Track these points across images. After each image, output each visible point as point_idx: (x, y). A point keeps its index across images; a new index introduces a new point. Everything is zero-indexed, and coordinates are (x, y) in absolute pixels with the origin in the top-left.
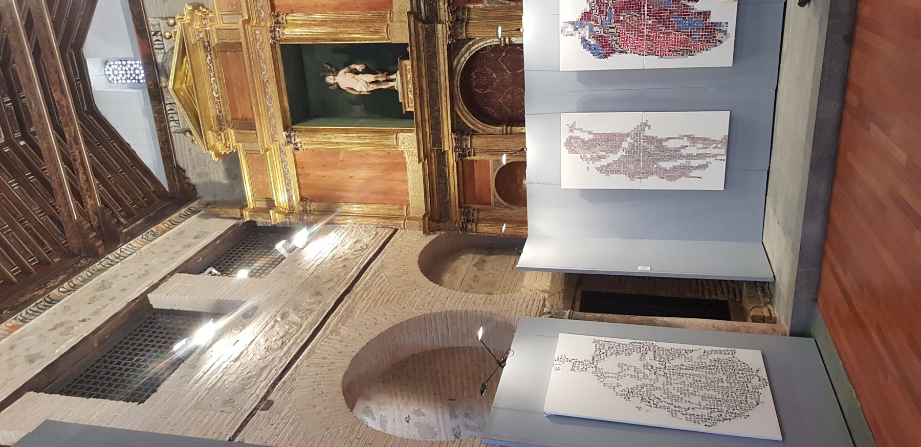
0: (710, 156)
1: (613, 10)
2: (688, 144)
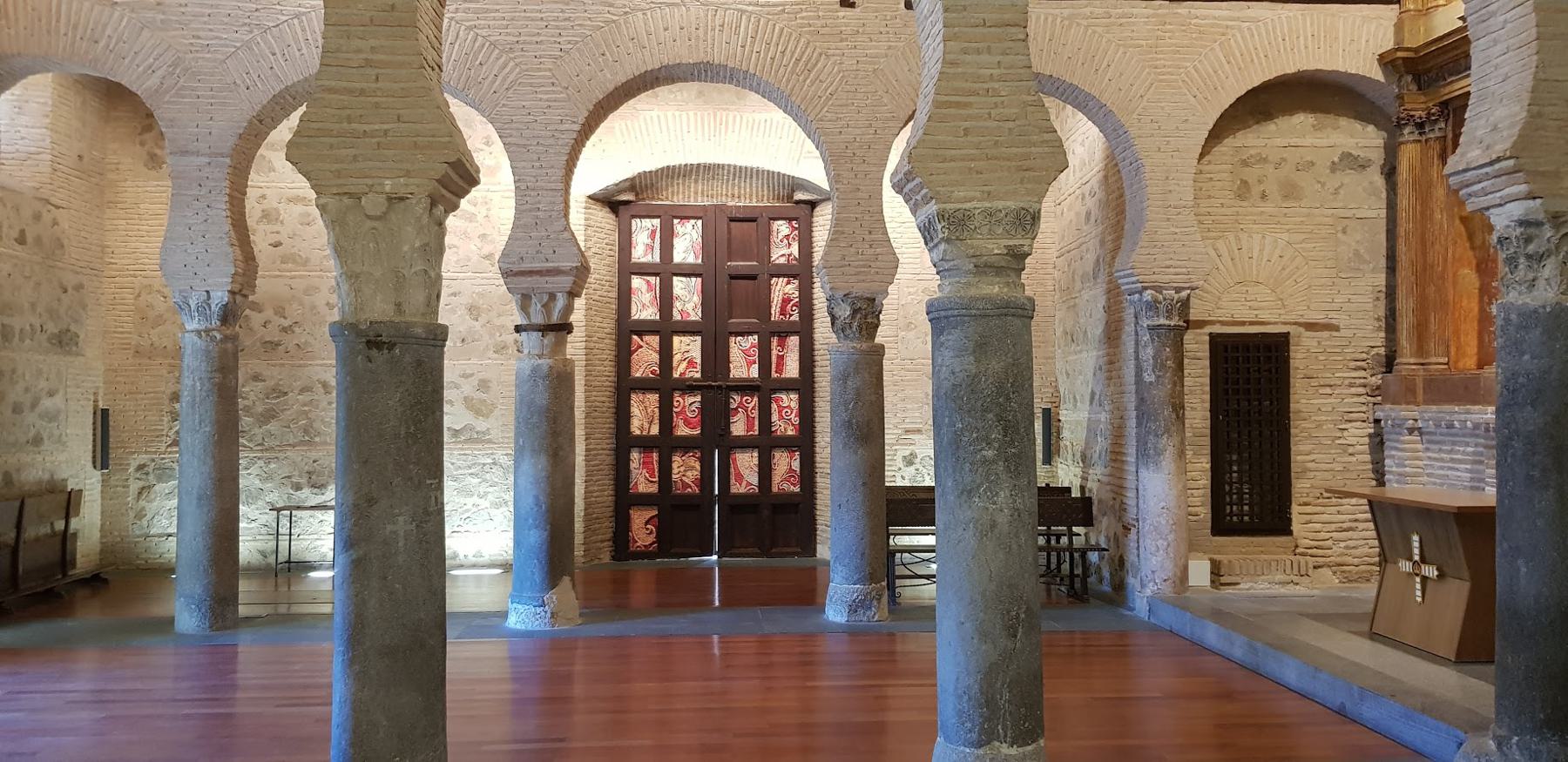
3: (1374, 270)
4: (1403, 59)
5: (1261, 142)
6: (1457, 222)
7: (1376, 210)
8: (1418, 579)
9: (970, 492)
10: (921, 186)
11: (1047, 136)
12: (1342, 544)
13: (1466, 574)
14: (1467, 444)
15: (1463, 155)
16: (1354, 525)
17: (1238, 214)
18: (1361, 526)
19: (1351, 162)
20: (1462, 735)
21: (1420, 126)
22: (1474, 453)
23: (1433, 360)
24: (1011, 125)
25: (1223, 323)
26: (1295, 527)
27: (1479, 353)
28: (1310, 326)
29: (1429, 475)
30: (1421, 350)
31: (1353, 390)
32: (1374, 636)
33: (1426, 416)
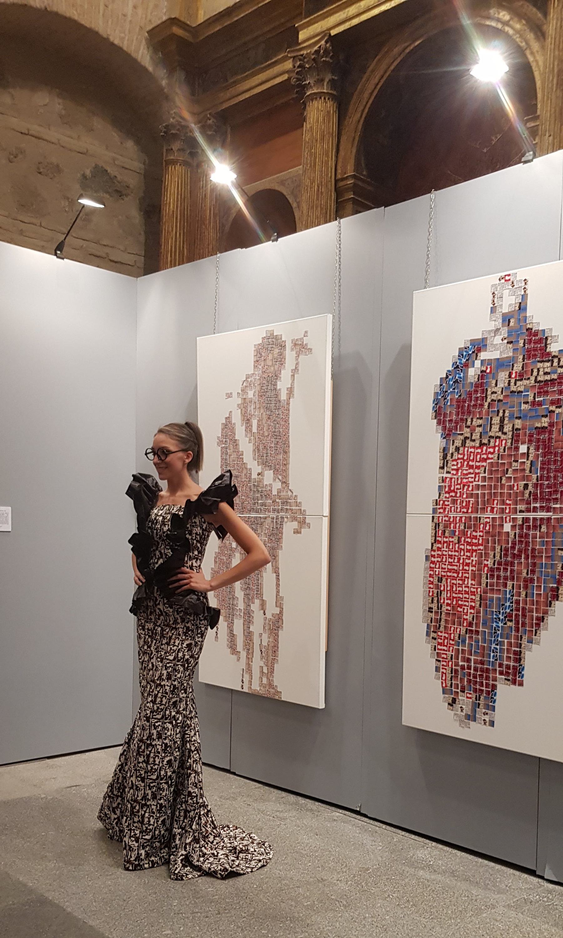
0: (249, 658)
1: (545, 422)
2: (269, 616)
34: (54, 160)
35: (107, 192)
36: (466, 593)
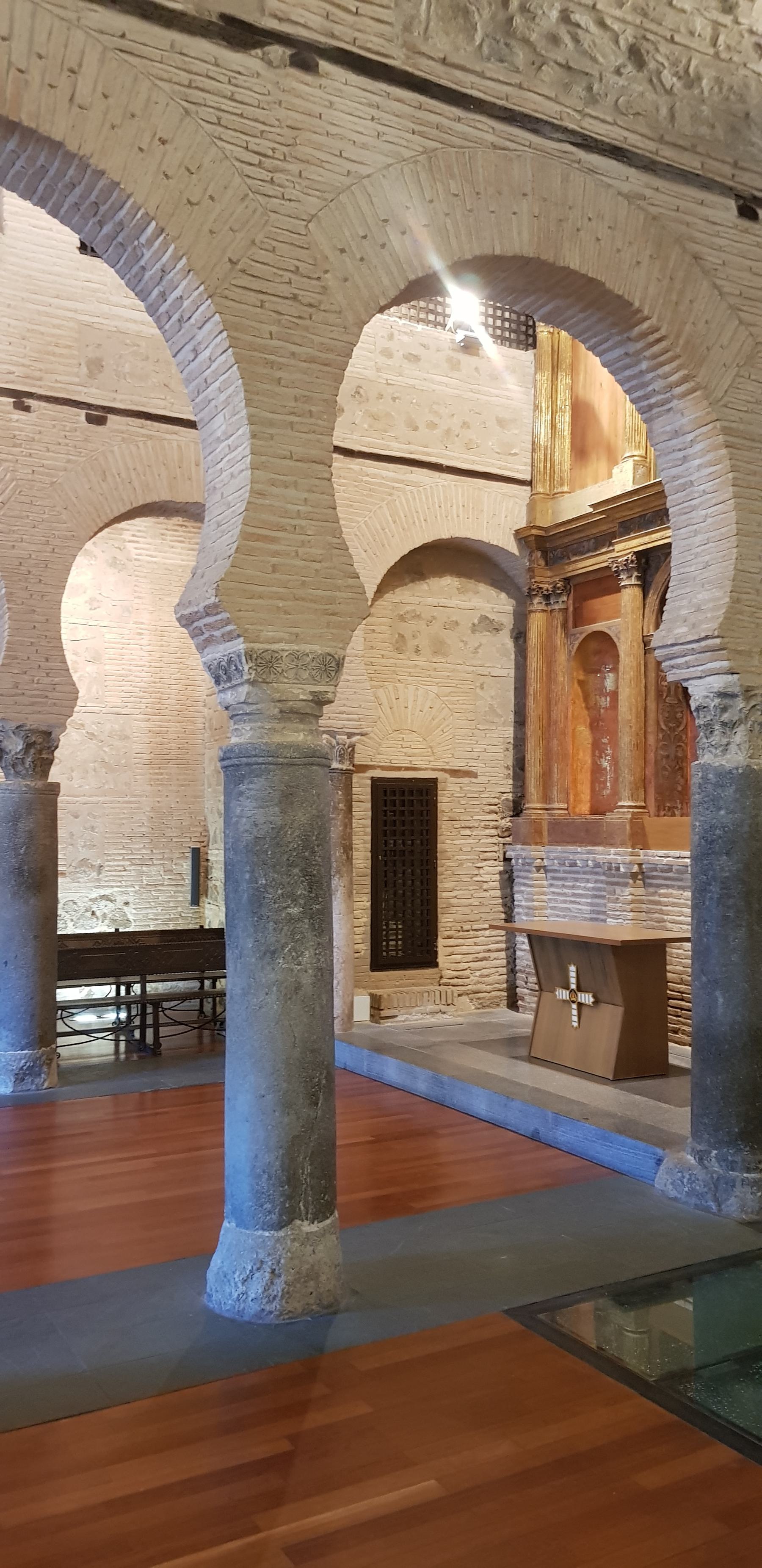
3: (504, 724)
4: (536, 536)
5: (417, 600)
6: (576, 685)
7: (506, 669)
8: (574, 1006)
9: (274, 953)
10: (228, 622)
11: (351, 581)
12: (478, 973)
13: (619, 999)
14: (588, 881)
15: (670, 630)
16: (487, 955)
17: (396, 665)
18: (493, 955)
19: (487, 624)
20: (659, 1151)
21: (547, 597)
22: (593, 889)
23: (556, 805)
24: (317, 566)
25: (383, 768)
26: (441, 959)
27: (592, 797)
28: (455, 773)
29: (552, 908)
30: (546, 798)
31: (488, 832)
32: (532, 1059)
33: (552, 855)
34: (454, 619)
35: (489, 631)
36: (404, 903)
